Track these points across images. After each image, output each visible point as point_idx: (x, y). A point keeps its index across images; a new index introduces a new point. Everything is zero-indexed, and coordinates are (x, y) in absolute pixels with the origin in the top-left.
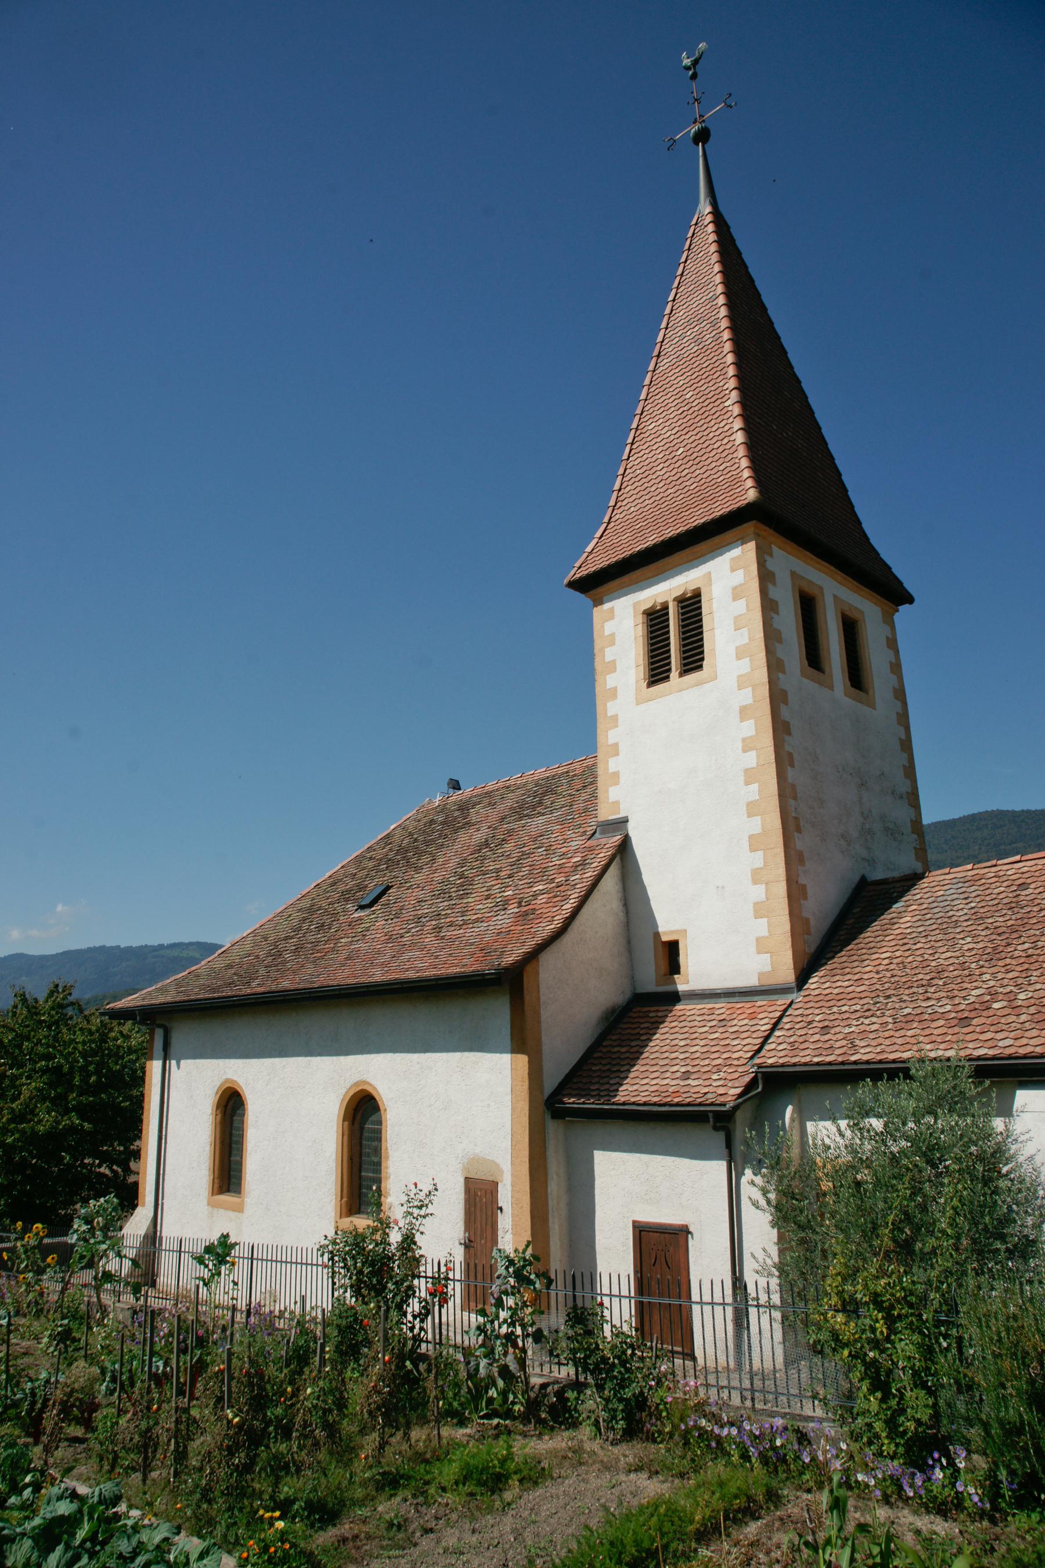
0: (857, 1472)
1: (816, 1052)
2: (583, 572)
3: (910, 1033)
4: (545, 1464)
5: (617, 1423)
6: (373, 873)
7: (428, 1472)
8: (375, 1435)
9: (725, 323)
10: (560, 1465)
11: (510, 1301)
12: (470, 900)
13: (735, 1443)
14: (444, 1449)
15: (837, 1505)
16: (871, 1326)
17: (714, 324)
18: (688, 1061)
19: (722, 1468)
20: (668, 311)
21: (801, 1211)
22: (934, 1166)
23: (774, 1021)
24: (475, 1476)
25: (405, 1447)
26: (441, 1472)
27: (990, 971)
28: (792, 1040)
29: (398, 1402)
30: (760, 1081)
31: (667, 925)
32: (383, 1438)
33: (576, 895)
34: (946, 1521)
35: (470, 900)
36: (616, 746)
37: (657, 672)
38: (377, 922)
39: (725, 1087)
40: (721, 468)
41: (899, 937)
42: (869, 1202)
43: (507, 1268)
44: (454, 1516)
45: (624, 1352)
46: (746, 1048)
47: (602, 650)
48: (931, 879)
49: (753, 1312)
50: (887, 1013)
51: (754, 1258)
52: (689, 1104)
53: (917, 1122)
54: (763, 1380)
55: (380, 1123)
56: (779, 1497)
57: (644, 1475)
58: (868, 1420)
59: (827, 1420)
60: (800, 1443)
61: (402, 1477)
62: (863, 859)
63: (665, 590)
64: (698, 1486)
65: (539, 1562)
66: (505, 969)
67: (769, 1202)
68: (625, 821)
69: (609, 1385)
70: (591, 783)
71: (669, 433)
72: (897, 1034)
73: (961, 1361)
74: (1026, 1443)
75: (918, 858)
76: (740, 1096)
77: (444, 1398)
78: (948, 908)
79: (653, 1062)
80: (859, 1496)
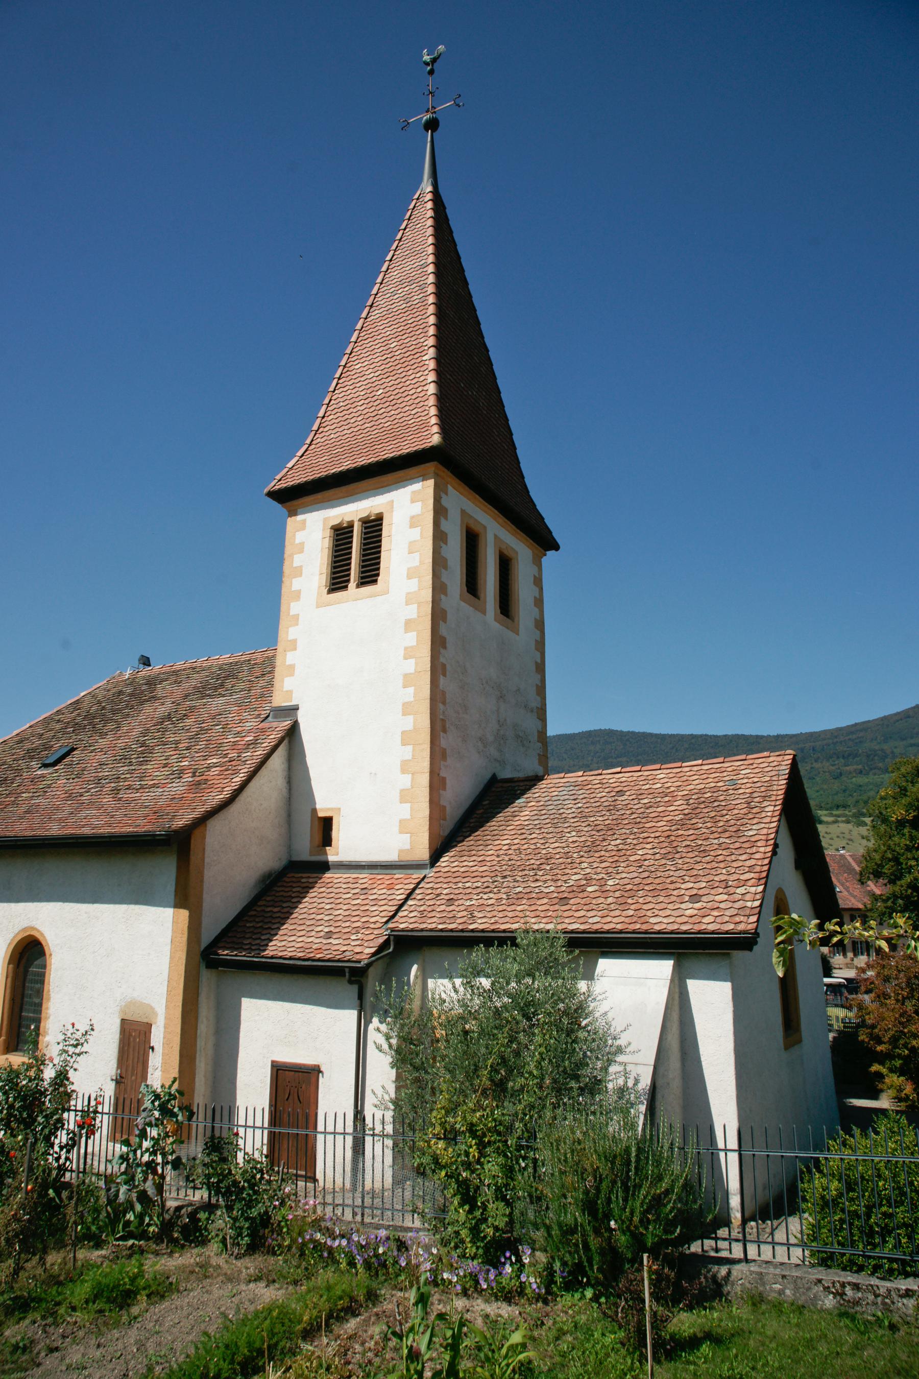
0: (443, 1271)
1: (441, 921)
2: (283, 485)
3: (519, 908)
4: (173, 1279)
5: (242, 1239)
6: (60, 735)
7: (59, 1294)
8: (11, 1262)
9: (431, 289)
10: (187, 1280)
11: (154, 1132)
12: (149, 767)
13: (344, 1252)
14: (78, 1271)
15: (423, 1300)
16: (465, 1151)
17: (422, 288)
18: (331, 923)
19: (331, 1274)
20: (384, 268)
21: (417, 1055)
22: (529, 1019)
23: (408, 891)
24: (105, 1294)
25: (39, 1271)
26: (73, 1293)
27: (588, 860)
28: (422, 908)
29: (37, 1229)
30: (392, 943)
31: (324, 804)
32: (17, 1264)
33: (246, 770)
34: (510, 1305)
35: (149, 767)
36: (294, 642)
37: (338, 581)
38: (59, 781)
39: (361, 947)
40: (413, 412)
41: (518, 828)
42: (473, 1048)
43: (153, 1102)
44: (81, 1333)
45: (254, 1177)
46: (383, 914)
47: (292, 556)
48: (549, 781)
49: (369, 1140)
50: (503, 890)
51: (374, 1094)
52: (329, 960)
53: (519, 982)
54: (373, 1198)
55: (44, 966)
56: (377, 1296)
57: (262, 1284)
58: (456, 1229)
59: (424, 1230)
60: (399, 1250)
61: (33, 1300)
62: (495, 760)
63: (353, 511)
64: (309, 1291)
65: (158, 1369)
66: (175, 831)
67: (390, 1046)
68: (295, 709)
69: (237, 1206)
70: (270, 672)
71: (372, 375)
72: (509, 909)
73: (534, 1177)
74: (577, 1240)
75: (540, 763)
76: (374, 954)
77: (82, 1223)
78: (560, 806)
79: (301, 922)
80: (443, 1291)
